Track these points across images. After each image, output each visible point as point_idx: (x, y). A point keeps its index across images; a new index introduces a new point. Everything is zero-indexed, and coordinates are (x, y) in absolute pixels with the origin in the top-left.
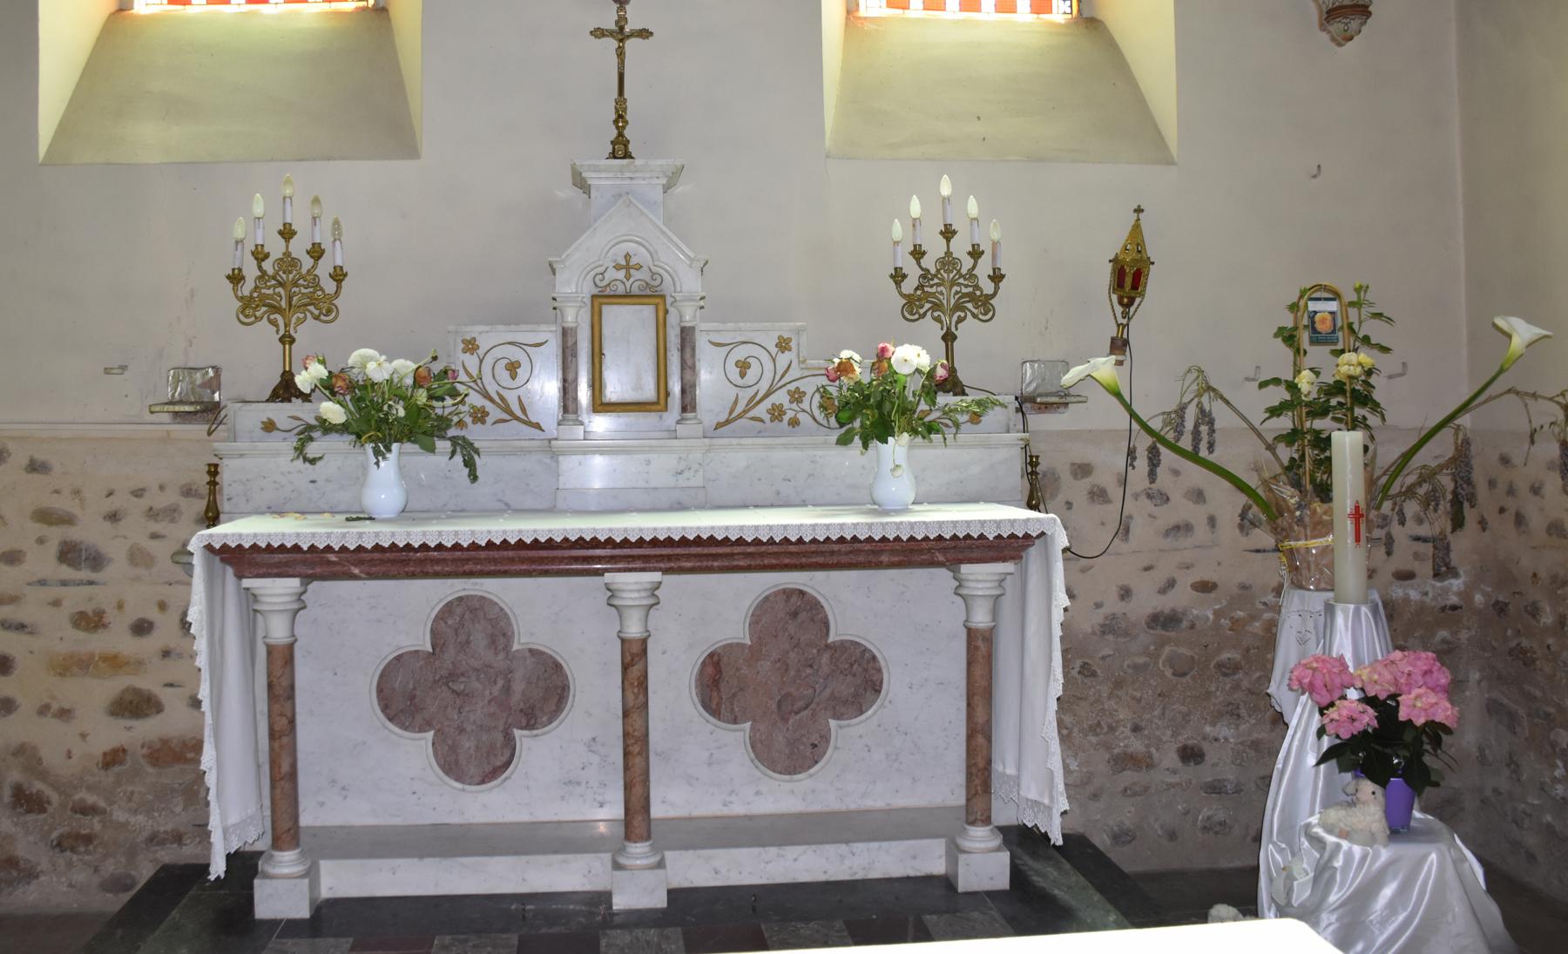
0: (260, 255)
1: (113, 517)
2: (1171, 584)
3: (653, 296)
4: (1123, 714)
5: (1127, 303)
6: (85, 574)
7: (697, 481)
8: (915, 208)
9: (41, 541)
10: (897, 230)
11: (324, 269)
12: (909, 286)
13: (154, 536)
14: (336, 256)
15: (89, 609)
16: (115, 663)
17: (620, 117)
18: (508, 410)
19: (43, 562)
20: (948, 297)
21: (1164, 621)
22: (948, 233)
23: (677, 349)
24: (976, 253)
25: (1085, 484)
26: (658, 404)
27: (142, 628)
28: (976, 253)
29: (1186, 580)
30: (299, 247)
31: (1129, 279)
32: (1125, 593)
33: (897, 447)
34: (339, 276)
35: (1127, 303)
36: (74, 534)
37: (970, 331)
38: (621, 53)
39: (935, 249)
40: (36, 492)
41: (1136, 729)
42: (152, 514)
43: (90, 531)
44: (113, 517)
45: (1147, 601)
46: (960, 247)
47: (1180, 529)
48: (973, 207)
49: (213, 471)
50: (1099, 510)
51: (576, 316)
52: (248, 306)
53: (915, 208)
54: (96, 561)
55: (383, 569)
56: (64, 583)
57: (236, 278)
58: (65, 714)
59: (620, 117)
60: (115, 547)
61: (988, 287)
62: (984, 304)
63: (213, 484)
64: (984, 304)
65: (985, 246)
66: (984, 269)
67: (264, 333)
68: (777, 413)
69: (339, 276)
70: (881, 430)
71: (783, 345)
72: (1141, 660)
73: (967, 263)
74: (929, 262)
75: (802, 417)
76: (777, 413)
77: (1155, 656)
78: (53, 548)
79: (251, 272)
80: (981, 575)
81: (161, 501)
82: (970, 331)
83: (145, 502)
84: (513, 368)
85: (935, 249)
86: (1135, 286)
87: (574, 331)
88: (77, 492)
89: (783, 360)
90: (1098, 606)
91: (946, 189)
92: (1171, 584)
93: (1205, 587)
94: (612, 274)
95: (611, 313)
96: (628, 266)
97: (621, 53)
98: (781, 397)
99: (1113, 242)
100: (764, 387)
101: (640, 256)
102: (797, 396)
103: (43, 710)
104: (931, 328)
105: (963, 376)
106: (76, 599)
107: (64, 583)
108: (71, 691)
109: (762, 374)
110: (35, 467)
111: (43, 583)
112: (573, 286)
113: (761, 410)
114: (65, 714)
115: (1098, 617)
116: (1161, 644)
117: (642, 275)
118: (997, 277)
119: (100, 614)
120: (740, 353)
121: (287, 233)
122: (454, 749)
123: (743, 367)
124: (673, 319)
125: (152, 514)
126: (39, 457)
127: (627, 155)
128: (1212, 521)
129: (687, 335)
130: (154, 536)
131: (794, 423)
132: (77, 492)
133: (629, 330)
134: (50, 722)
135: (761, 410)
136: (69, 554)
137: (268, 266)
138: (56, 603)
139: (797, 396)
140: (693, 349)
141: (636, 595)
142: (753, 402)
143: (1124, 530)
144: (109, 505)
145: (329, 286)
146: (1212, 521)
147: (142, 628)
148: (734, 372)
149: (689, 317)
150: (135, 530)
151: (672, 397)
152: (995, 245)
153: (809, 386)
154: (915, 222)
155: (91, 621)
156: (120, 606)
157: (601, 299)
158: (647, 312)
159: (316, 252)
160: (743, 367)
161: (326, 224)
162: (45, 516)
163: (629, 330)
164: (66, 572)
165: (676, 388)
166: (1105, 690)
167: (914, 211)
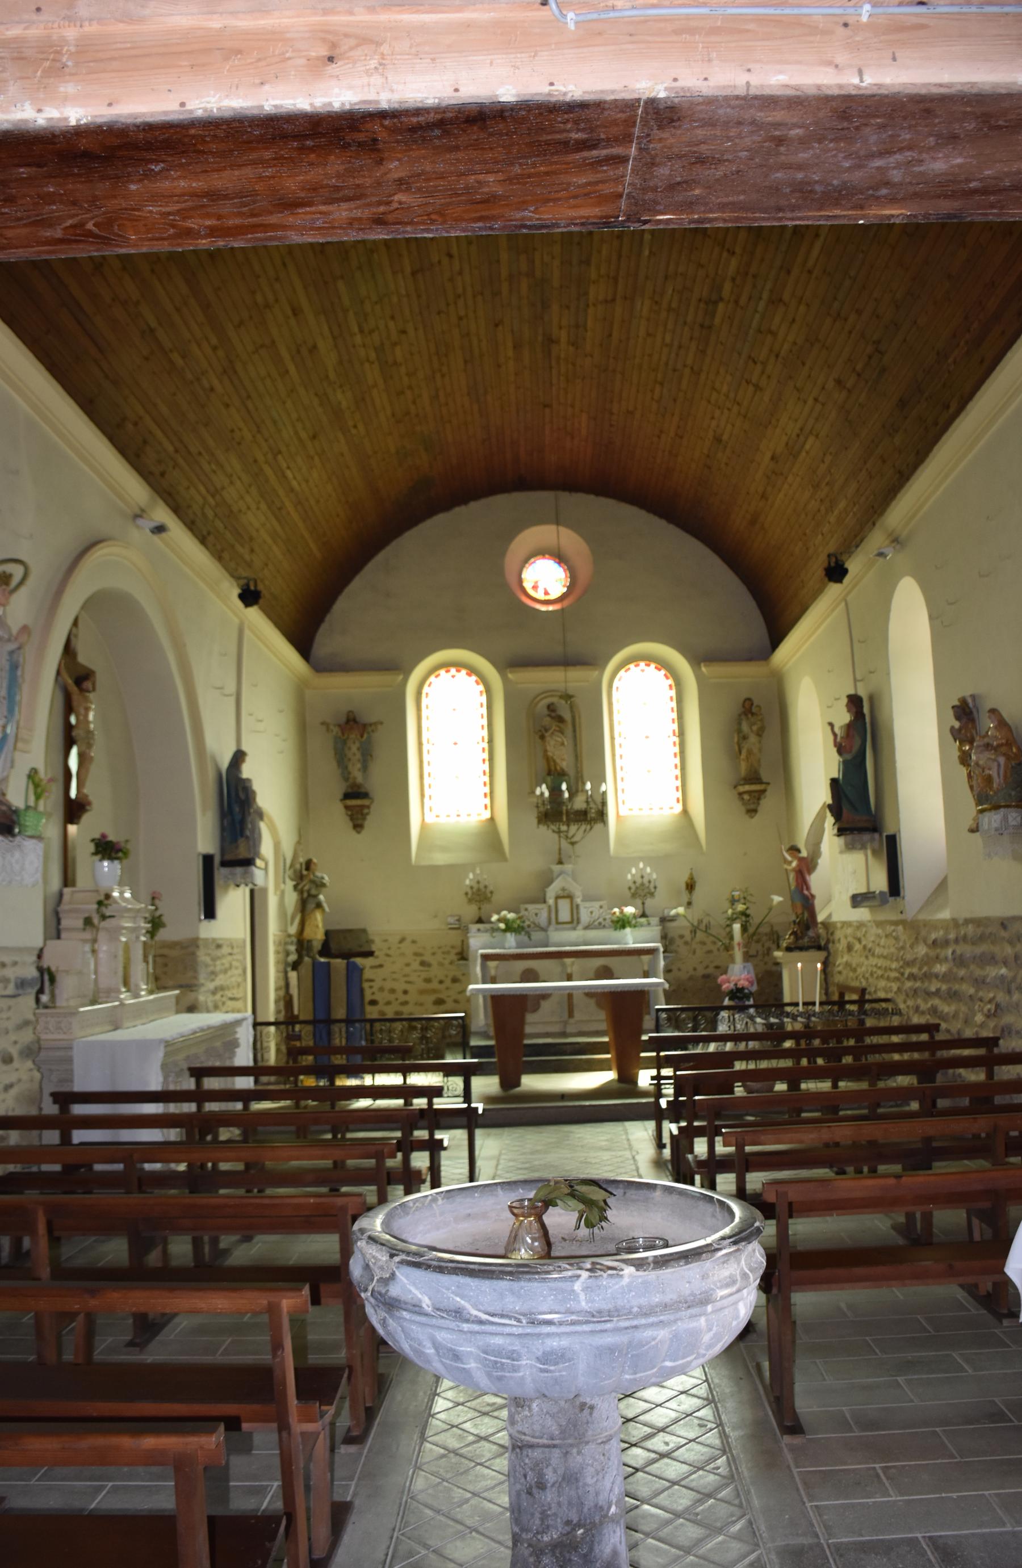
0: (472, 888)
3: (570, 897)
8: (634, 871)
12: (633, 891)
14: (491, 888)
16: (434, 991)
17: (560, 854)
19: (415, 965)
21: (706, 977)
22: (642, 877)
23: (575, 909)
26: (572, 922)
27: (441, 982)
28: (650, 882)
31: (690, 887)
32: (695, 969)
33: (628, 930)
34: (492, 892)
36: (424, 958)
37: (649, 902)
42: (443, 953)
43: (427, 958)
44: (434, 954)
47: (710, 952)
48: (648, 870)
51: (551, 901)
52: (470, 901)
53: (634, 871)
54: (429, 965)
55: (858, 538)
57: (466, 894)
58: (421, 1004)
59: (560, 854)
60: (434, 962)
61: (653, 890)
62: (652, 894)
64: (652, 894)
66: (652, 886)
69: (492, 892)
70: (623, 927)
78: (418, 962)
80: (645, 958)
82: (649, 902)
84: (536, 914)
87: (264, 891)
92: (707, 967)
98: (601, 920)
99: (685, 878)
102: (605, 919)
103: (416, 1004)
104: (639, 902)
105: (647, 912)
106: (424, 975)
109: (596, 915)
110: (414, 942)
111: (415, 971)
114: (421, 1004)
123: (592, 913)
125: (443, 953)
129: (578, 906)
136: (423, 963)
141: (660, 1417)
145: (489, 895)
147: (441, 982)
153: (607, 917)
155: (428, 980)
160: (592, 913)
162: (416, 954)
164: (422, 968)
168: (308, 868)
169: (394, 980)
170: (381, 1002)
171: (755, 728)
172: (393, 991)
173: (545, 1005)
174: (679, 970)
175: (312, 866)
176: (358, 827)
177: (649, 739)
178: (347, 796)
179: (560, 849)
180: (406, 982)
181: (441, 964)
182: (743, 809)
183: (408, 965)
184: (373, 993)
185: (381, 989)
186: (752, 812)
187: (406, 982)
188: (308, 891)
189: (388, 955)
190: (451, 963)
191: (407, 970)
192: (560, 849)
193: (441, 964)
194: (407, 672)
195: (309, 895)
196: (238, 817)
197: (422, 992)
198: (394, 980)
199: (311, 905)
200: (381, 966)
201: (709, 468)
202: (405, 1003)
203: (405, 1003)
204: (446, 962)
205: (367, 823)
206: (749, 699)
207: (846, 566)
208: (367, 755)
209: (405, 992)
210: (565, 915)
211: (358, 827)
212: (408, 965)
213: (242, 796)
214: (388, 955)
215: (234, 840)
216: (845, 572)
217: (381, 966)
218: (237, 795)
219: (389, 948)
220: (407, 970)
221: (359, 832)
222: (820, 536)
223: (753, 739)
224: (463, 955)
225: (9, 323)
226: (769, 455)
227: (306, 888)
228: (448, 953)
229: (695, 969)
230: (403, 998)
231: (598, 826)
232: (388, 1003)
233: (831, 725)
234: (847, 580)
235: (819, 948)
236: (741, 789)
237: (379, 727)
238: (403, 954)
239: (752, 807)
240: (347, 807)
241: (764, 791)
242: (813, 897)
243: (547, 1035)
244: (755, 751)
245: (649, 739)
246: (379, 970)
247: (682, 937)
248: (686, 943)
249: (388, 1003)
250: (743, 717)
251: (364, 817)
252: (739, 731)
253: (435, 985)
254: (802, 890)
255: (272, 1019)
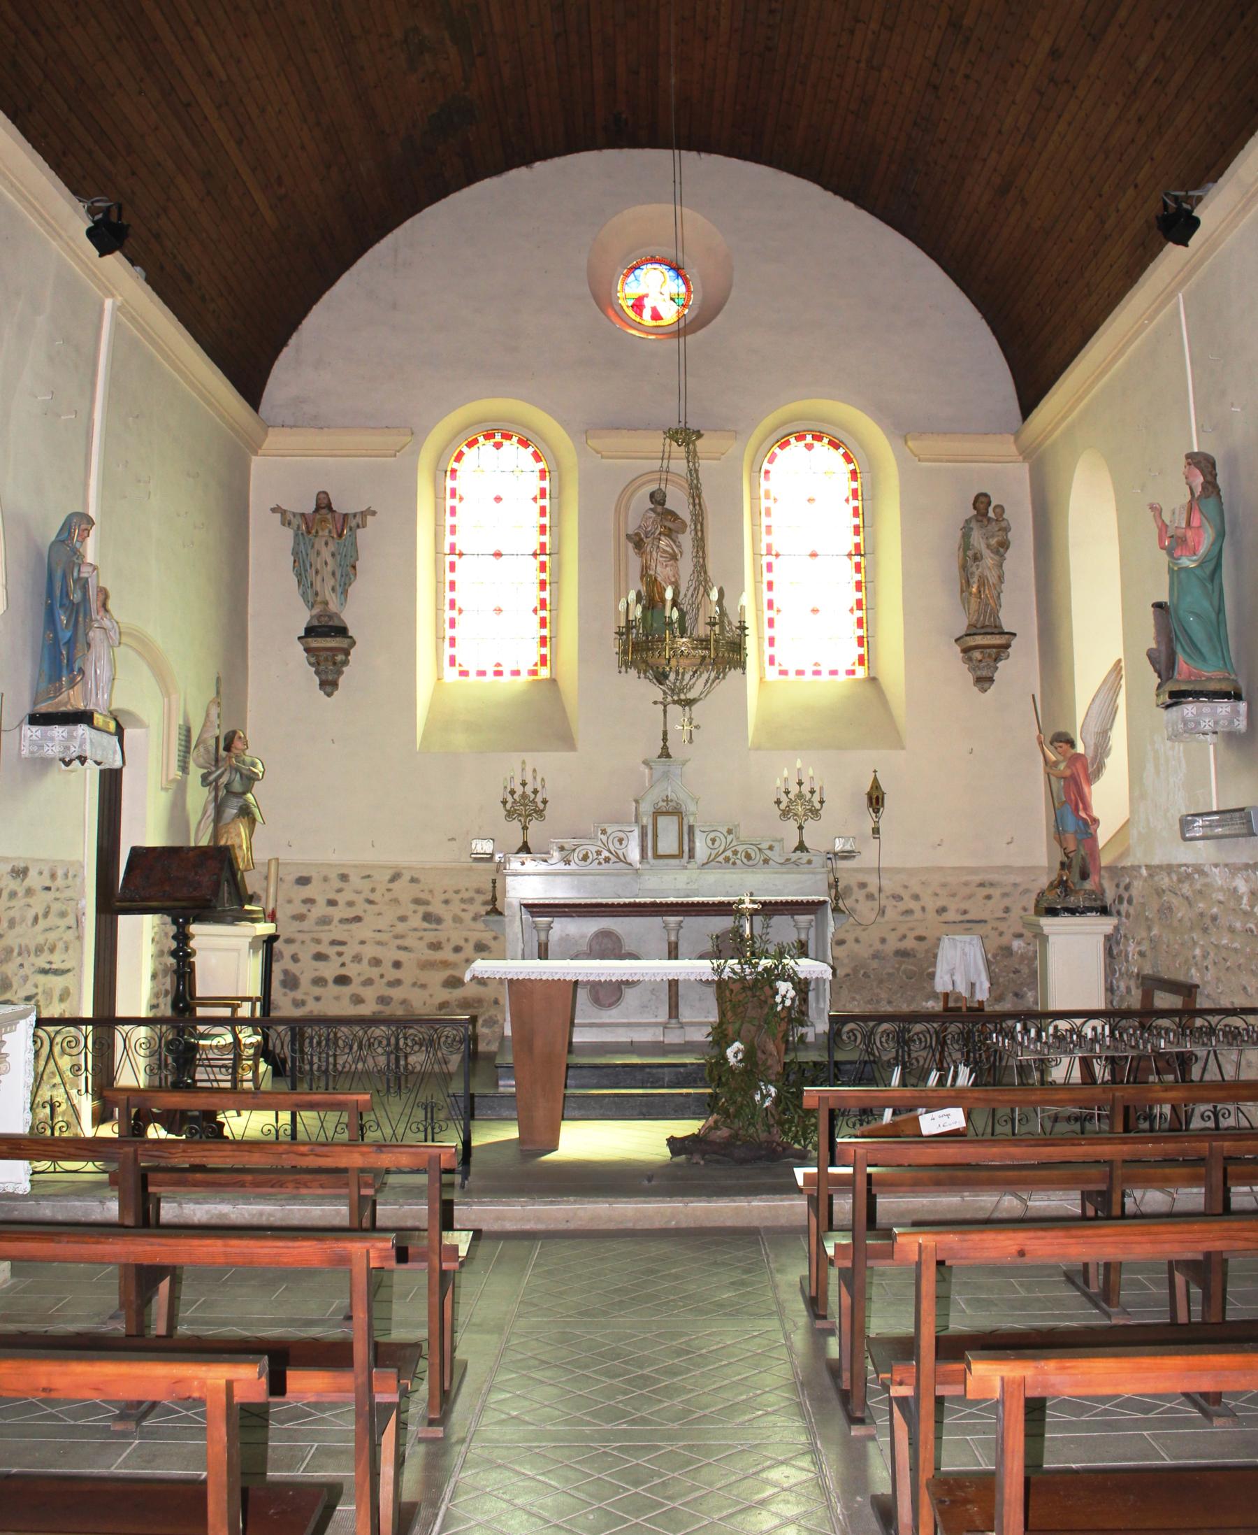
1: (446, 902)
2: (904, 937)
3: (677, 812)
4: (884, 995)
5: (876, 811)
6: (434, 926)
7: (695, 886)
9: (415, 912)
10: (779, 782)
11: (539, 799)
12: (783, 806)
13: (464, 910)
15: (434, 941)
16: (445, 964)
17: (665, 739)
18: (618, 857)
19: (416, 921)
20: (800, 809)
21: (903, 954)
23: (687, 833)
24: (812, 792)
25: (863, 892)
26: (679, 856)
27: (457, 949)
28: (812, 792)
29: (911, 935)
30: (529, 789)
32: (883, 941)
35: (876, 811)
36: (430, 909)
38: (665, 711)
39: (794, 790)
40: (415, 891)
41: (890, 1002)
42: (463, 901)
43: (437, 908)
44: (446, 902)
45: (893, 944)
46: (805, 789)
47: (909, 912)
49: (494, 882)
50: (870, 903)
51: (647, 820)
52: (510, 814)
54: (439, 920)
56: (425, 930)
58: (423, 986)
59: (665, 739)
61: (818, 806)
62: (815, 813)
63: (494, 887)
65: (817, 789)
67: (516, 825)
68: (727, 859)
69: (545, 802)
71: (730, 832)
72: (891, 971)
73: (809, 795)
74: (791, 796)
75: (738, 862)
76: (727, 859)
77: (898, 969)
78: (420, 915)
79: (510, 799)
80: (803, 919)
81: (466, 895)
83: (460, 896)
84: (620, 841)
85: (794, 790)
86: (877, 803)
88: (431, 891)
89: (730, 838)
90: (871, 946)
91: (799, 764)
92: (904, 937)
93: (920, 938)
94: (661, 804)
95: (662, 820)
96: (667, 800)
97: (665, 711)
98: (729, 853)
100: (722, 848)
101: (672, 796)
102: (735, 853)
103: (414, 984)
105: (807, 844)
106: (430, 937)
107: (425, 930)
108: (425, 976)
110: (413, 880)
111: (415, 930)
112: (647, 808)
113: (721, 859)
114: (423, 986)
115: (871, 951)
116: (901, 963)
117: (673, 804)
118: (822, 802)
119: (440, 943)
120: (712, 835)
121: (524, 784)
122: (597, 992)
123: (713, 841)
124: (685, 821)
125: (463, 901)
126: (415, 876)
127: (668, 756)
128: (923, 909)
129: (691, 828)
130: (464, 910)
131: (734, 863)
132: (431, 891)
133: (668, 827)
134: (417, 990)
135: (721, 859)
136: (427, 917)
137: (516, 796)
138: (421, 938)
139: (735, 853)
140: (718, 1162)
142: (718, 855)
143: (882, 912)
144: (444, 897)
146: (923, 909)
147: (457, 949)
148: (710, 843)
149: (692, 822)
150: (456, 907)
151: (685, 853)
152: (821, 788)
153: (740, 849)
154: (786, 780)
155: (435, 946)
156: (448, 940)
157: (657, 813)
158: (675, 819)
159: (535, 792)
160: (713, 841)
161: (539, 780)
162: (417, 901)
163: (668, 827)
164: (426, 925)
165: (686, 848)
166: (875, 984)
167: (785, 771)
168: (228, 748)
169: (379, 943)
170: (356, 981)
171: (993, 542)
172: (376, 962)
173: (629, 994)
174: (857, 941)
175: (238, 744)
176: (329, 685)
177: (816, 558)
178: (311, 631)
179: (665, 733)
180: (399, 948)
181: (457, 919)
182: (970, 677)
183: (403, 919)
184: (343, 965)
185: (357, 958)
186: (984, 681)
187: (399, 948)
188: (227, 786)
189: (371, 902)
190: (475, 918)
191: (401, 927)
192: (665, 733)
193: (457, 919)
194: (417, 434)
195: (230, 792)
196: (65, 635)
197: (426, 965)
198: (379, 943)
199: (231, 811)
200: (358, 919)
201: (936, 88)
202: (398, 982)
203: (398, 982)
204: (467, 917)
205: (342, 680)
206: (985, 495)
207: (1195, 214)
208: (347, 571)
209: (397, 965)
210: (668, 844)
211: (329, 685)
212: (403, 919)
213: (76, 597)
214: (371, 902)
215: (55, 677)
216: (1195, 223)
217: (358, 919)
218: (66, 593)
219: (373, 890)
220: (401, 927)
221: (329, 695)
222: (1131, 192)
223: (989, 559)
224: (495, 910)
225: (14, 117)
226: (1046, 45)
227: (224, 780)
228: (471, 900)
229: (883, 941)
230: (393, 974)
231: (733, 674)
232: (368, 982)
233: (1156, 510)
234: (1195, 240)
235: (1104, 911)
236: (973, 641)
237: (369, 518)
238: (396, 901)
239: (984, 673)
240: (307, 650)
241: (1008, 646)
242: (1096, 821)
243: (632, 1048)
244: (993, 579)
245: (816, 558)
246: (354, 926)
247: (863, 885)
248: (870, 897)
249: (368, 982)
250: (973, 524)
251: (339, 667)
252: (966, 544)
253: (447, 954)
254: (1077, 809)
255: (144, 1013)
